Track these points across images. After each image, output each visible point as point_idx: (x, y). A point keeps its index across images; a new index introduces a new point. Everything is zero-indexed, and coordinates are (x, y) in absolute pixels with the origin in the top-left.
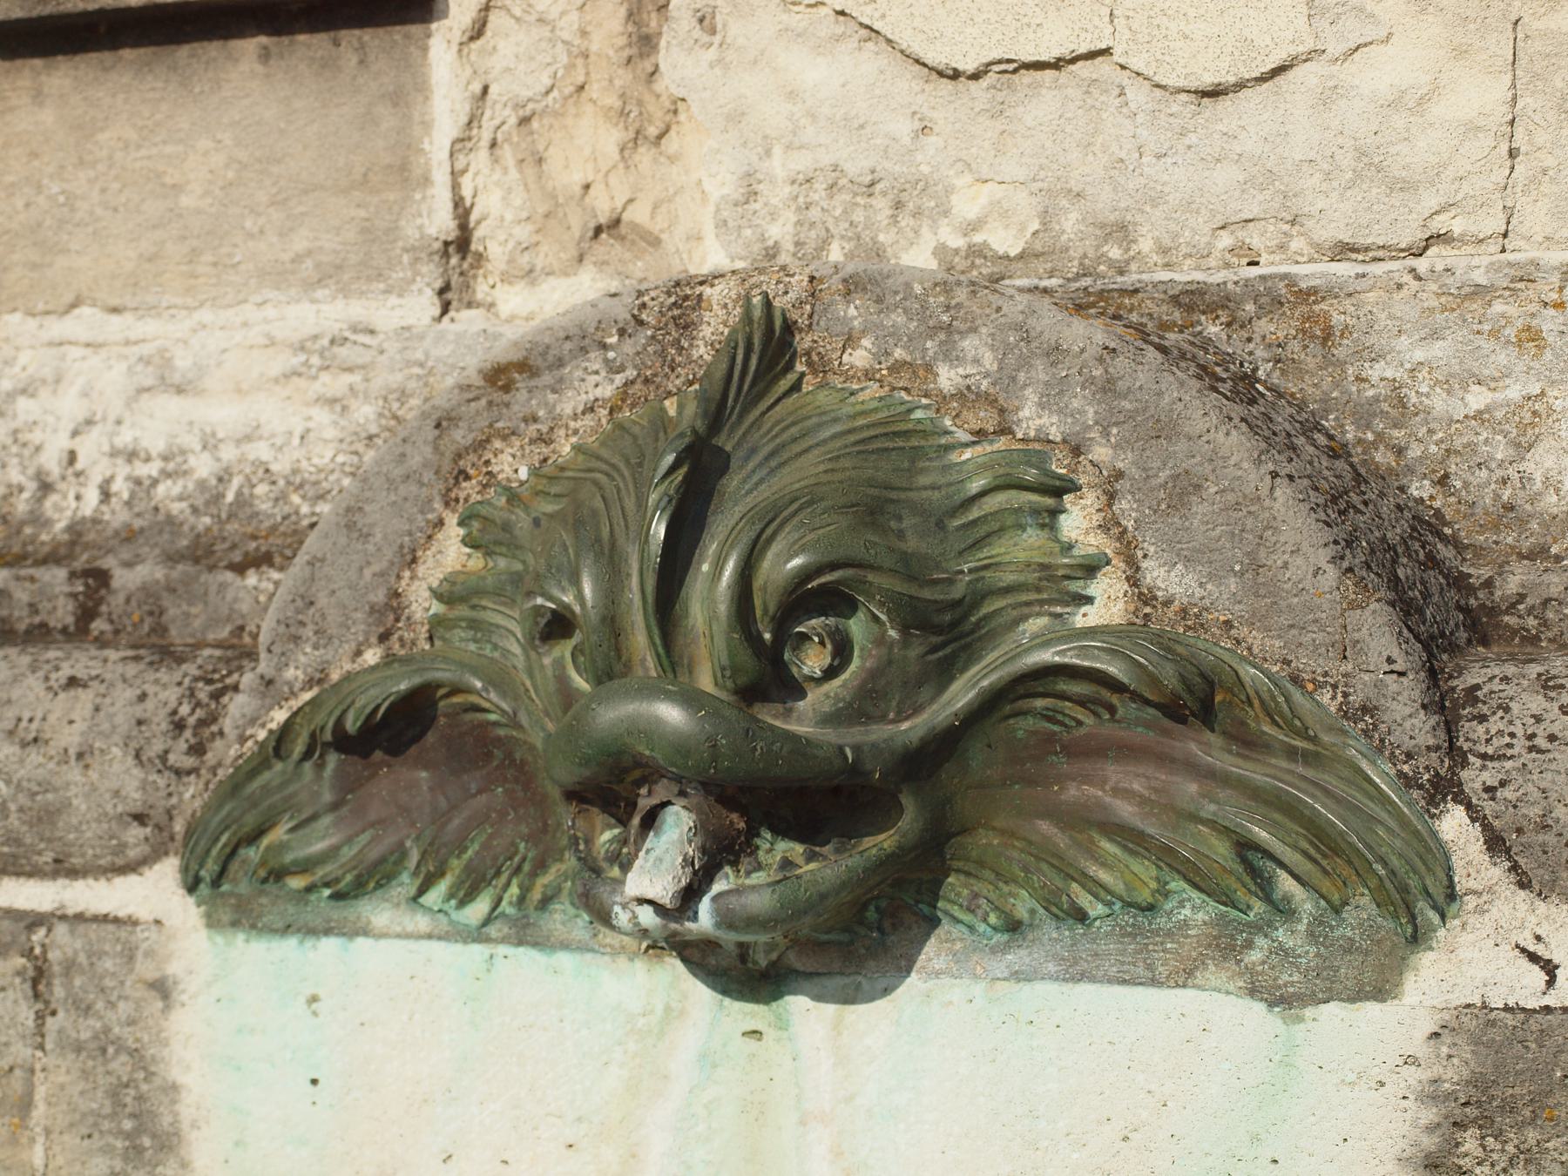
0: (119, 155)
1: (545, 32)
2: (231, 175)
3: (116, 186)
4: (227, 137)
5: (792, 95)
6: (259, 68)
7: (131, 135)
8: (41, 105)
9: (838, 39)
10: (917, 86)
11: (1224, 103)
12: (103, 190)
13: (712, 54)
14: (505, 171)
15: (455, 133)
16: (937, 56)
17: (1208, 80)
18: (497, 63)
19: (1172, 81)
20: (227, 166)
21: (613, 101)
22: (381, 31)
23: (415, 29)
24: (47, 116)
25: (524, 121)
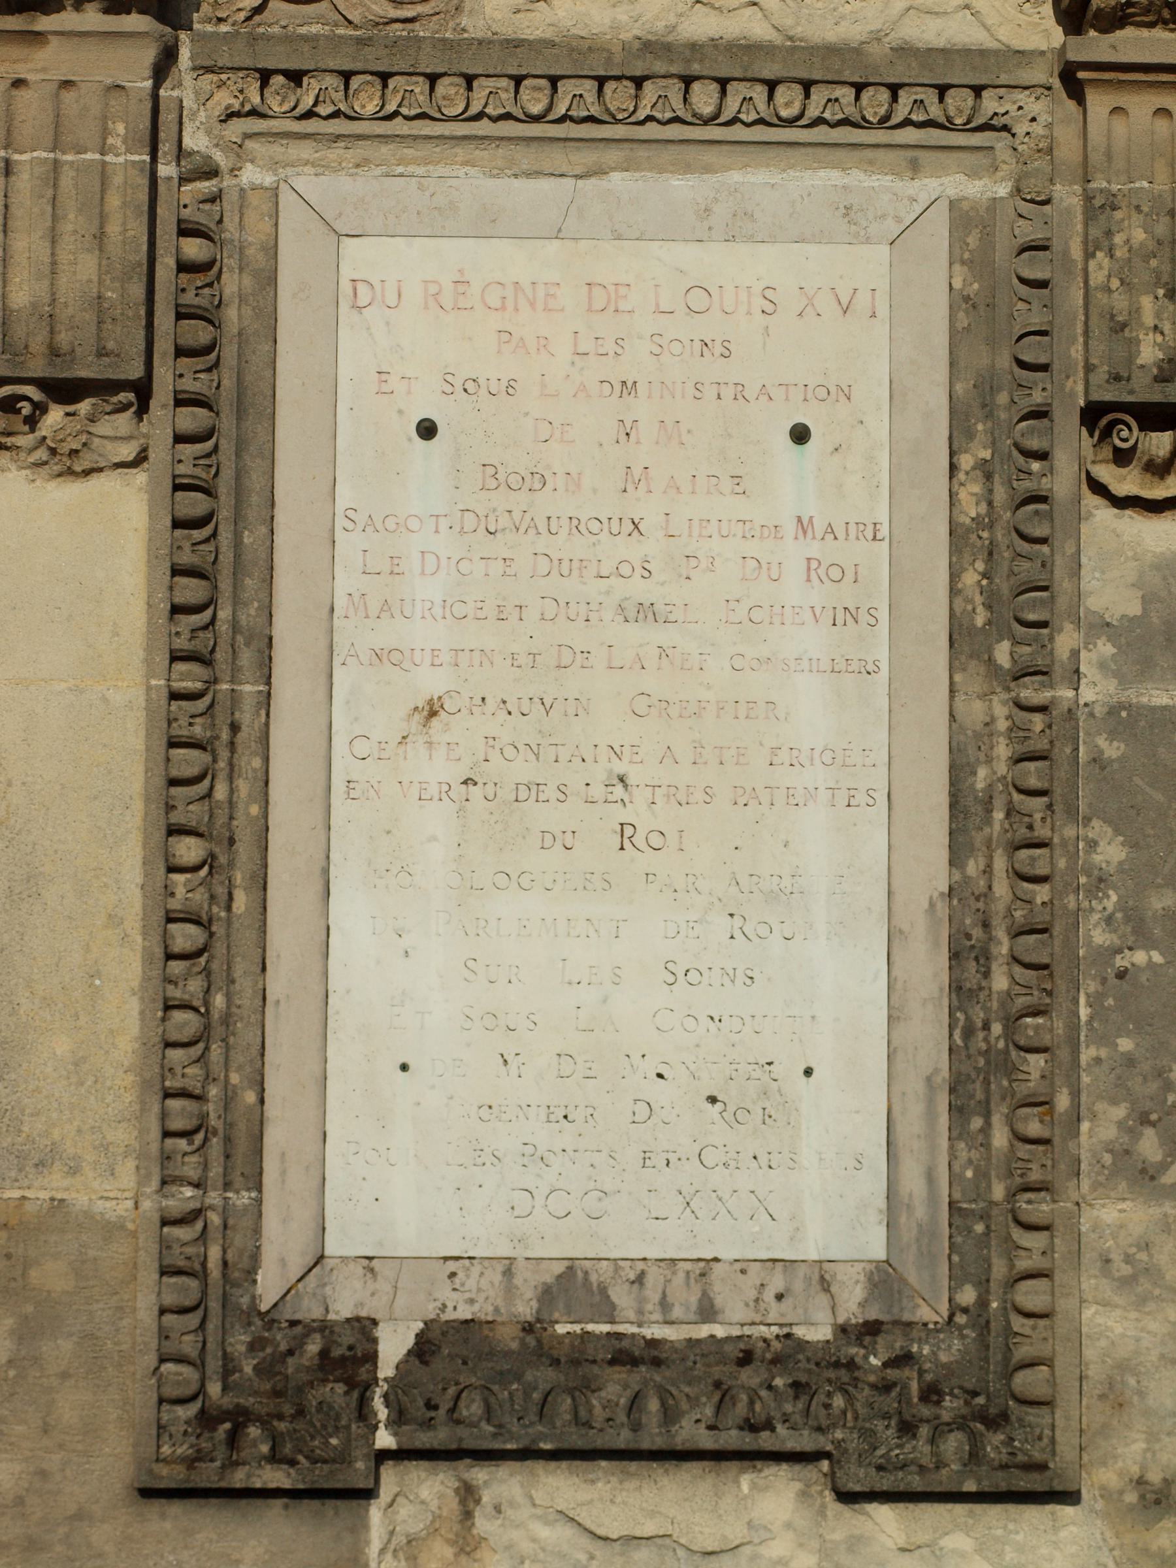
0: (207, 1545)
1: (424, 1507)
2: (266, 1557)
3: (204, 1559)
4: (265, 1541)
5: (534, 1540)
6: (283, 1512)
7: (215, 1537)
8: (164, 1520)
9: (556, 1521)
10: (588, 1541)
11: (713, 1557)
12: (198, 1560)
13: (499, 1522)
14: (399, 1561)
15: (381, 1546)
16: (601, 1532)
17: (710, 1549)
18: (399, 1518)
19: (695, 1548)
20: (265, 1553)
21: (451, 1536)
22: (346, 1502)
23: (363, 1502)
24: (168, 1525)
25: (409, 1542)
